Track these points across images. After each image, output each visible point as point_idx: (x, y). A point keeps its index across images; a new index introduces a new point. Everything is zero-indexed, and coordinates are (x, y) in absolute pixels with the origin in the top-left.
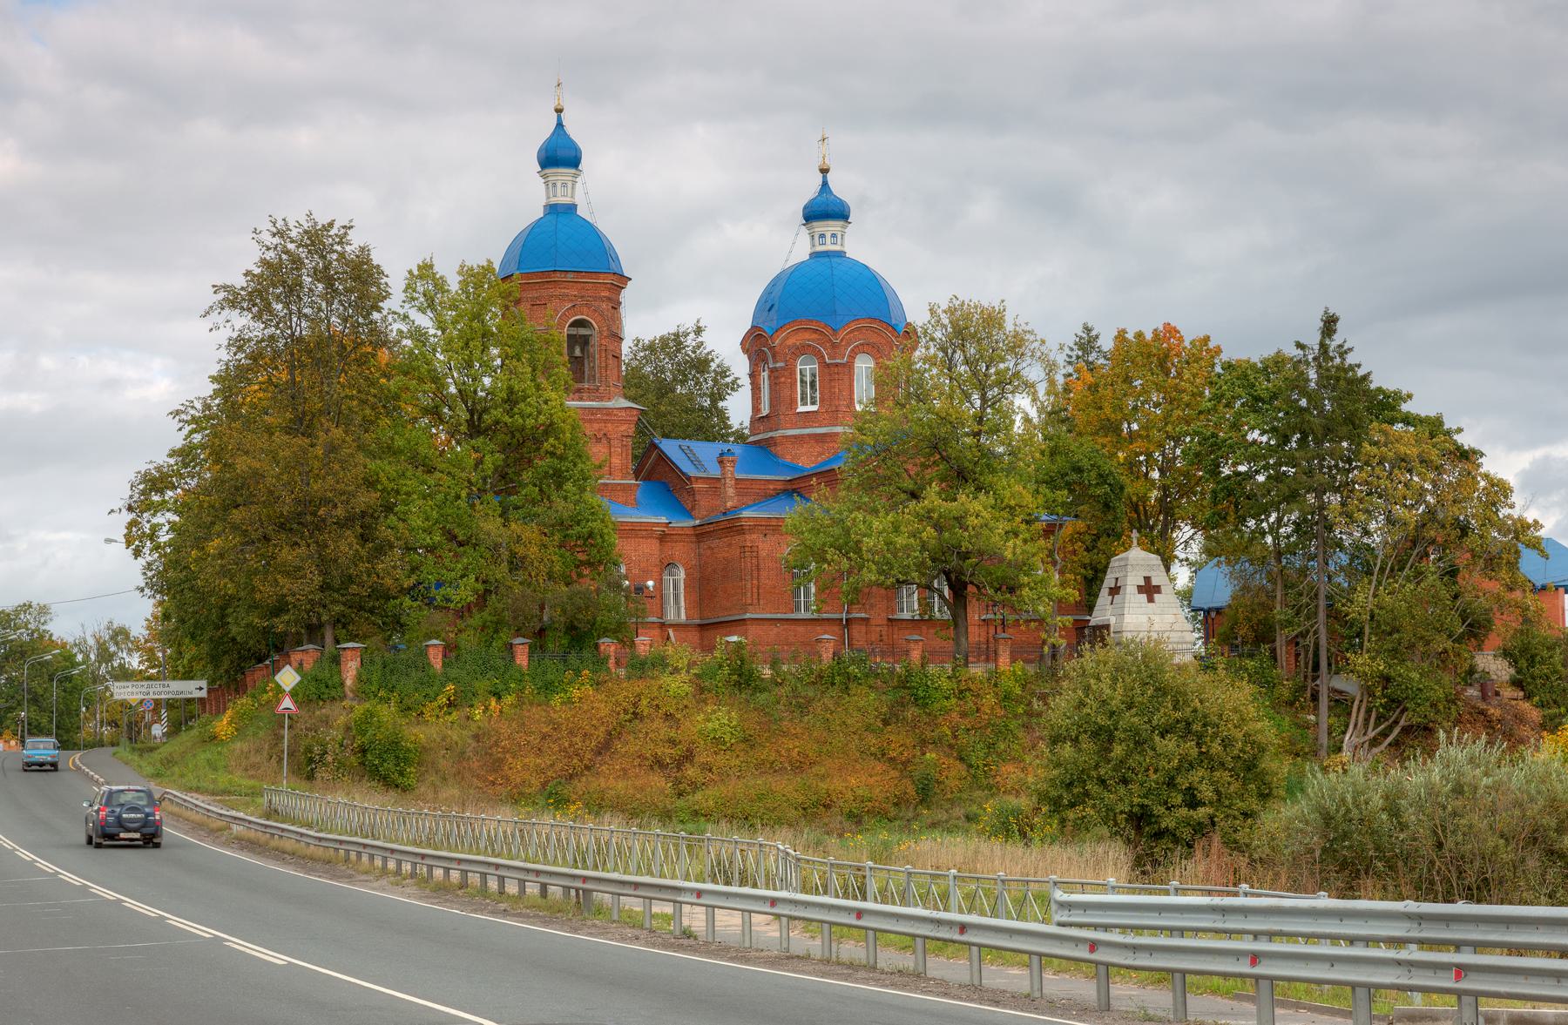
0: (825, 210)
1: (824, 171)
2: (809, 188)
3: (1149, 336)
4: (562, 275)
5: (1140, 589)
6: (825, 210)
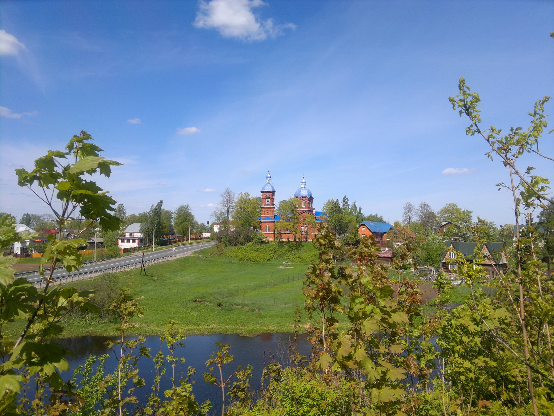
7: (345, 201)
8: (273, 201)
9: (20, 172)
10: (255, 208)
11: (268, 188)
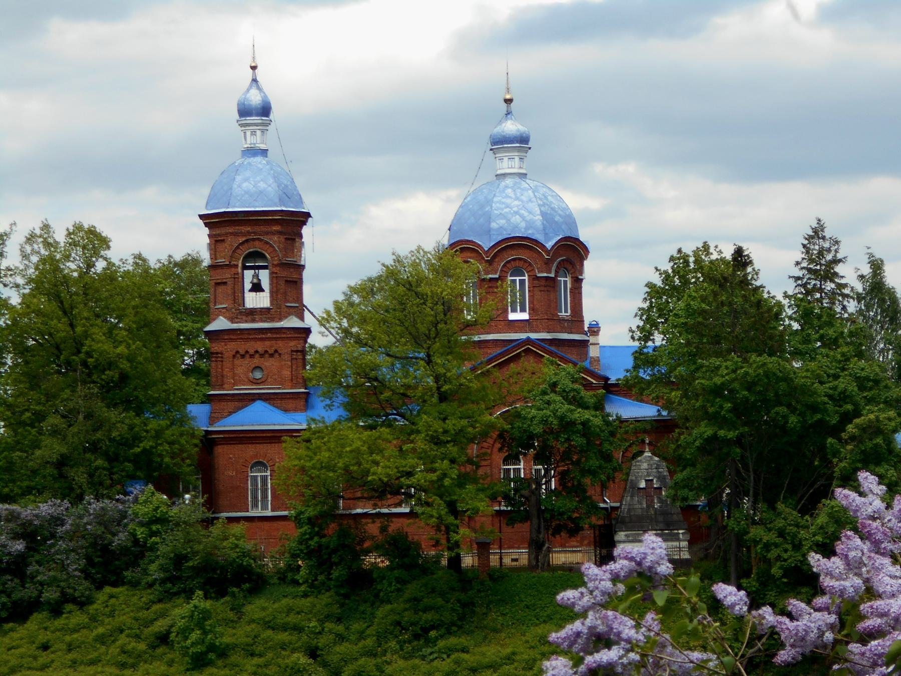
1: (254, 68)
7: (820, 262)
8: (296, 284)
9: (785, 293)
10: (148, 330)
11: (254, 192)
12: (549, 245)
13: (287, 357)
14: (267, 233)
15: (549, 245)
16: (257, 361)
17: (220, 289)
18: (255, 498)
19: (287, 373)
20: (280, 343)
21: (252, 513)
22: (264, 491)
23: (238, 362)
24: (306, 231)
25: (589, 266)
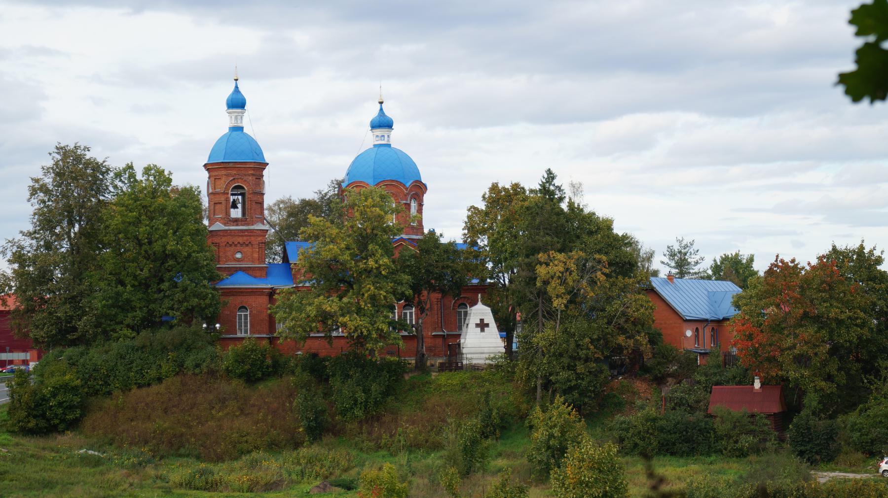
0: (383, 123)
1: (381, 103)
2: (373, 112)
3: (482, 206)
4: (239, 171)
5: (477, 325)
6: (383, 123)
12: (408, 185)
13: (256, 246)
14: (245, 175)
15: (408, 185)
16: (239, 248)
17: (218, 206)
18: (240, 326)
19: (256, 255)
20: (253, 238)
21: (239, 335)
22: (246, 323)
23: (228, 249)
24: (265, 173)
25: (426, 198)
